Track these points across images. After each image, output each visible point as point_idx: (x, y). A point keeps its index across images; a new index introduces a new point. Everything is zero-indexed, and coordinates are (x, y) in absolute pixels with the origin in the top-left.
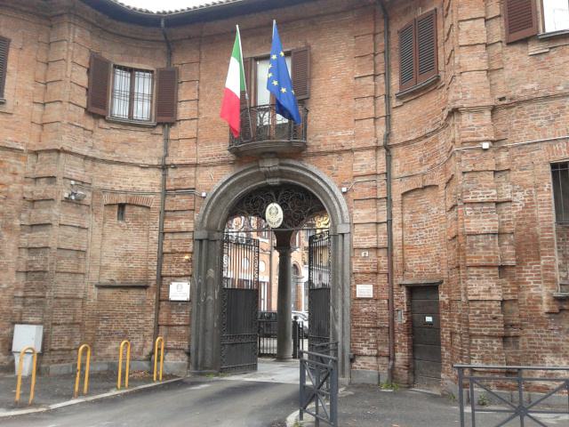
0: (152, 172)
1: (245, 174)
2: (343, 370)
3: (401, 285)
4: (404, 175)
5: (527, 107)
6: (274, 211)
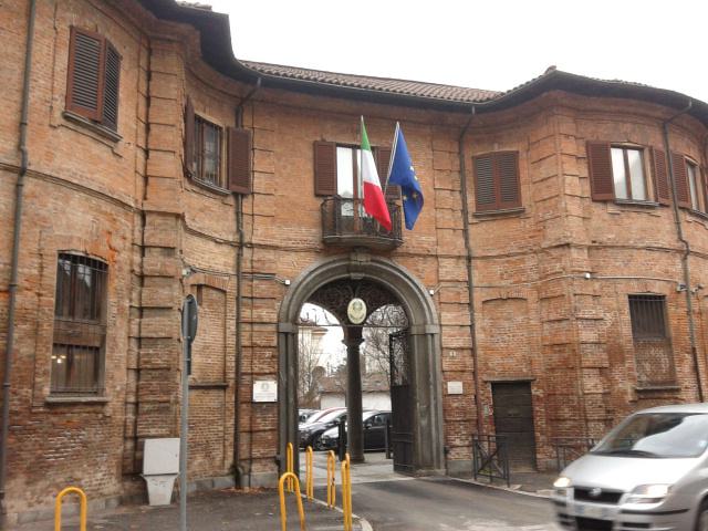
0: (225, 249)
1: (334, 266)
2: (439, 462)
3: (486, 382)
4: (483, 285)
5: (611, 251)
6: (357, 307)
